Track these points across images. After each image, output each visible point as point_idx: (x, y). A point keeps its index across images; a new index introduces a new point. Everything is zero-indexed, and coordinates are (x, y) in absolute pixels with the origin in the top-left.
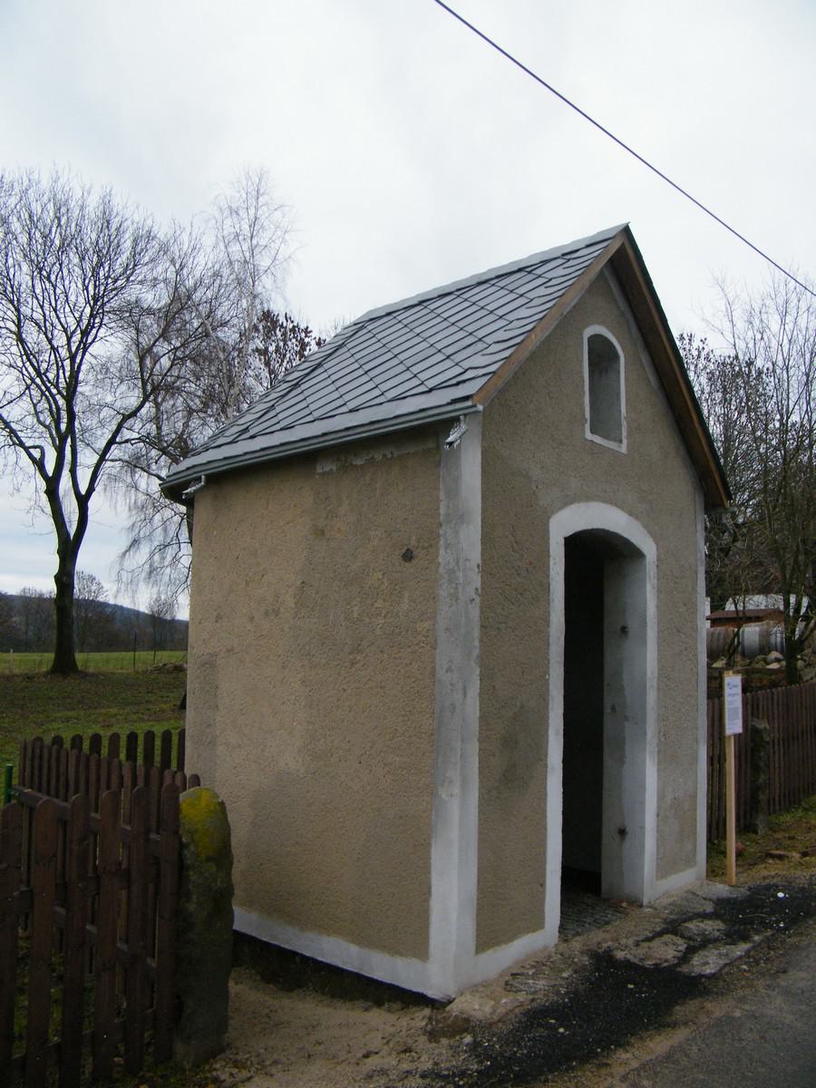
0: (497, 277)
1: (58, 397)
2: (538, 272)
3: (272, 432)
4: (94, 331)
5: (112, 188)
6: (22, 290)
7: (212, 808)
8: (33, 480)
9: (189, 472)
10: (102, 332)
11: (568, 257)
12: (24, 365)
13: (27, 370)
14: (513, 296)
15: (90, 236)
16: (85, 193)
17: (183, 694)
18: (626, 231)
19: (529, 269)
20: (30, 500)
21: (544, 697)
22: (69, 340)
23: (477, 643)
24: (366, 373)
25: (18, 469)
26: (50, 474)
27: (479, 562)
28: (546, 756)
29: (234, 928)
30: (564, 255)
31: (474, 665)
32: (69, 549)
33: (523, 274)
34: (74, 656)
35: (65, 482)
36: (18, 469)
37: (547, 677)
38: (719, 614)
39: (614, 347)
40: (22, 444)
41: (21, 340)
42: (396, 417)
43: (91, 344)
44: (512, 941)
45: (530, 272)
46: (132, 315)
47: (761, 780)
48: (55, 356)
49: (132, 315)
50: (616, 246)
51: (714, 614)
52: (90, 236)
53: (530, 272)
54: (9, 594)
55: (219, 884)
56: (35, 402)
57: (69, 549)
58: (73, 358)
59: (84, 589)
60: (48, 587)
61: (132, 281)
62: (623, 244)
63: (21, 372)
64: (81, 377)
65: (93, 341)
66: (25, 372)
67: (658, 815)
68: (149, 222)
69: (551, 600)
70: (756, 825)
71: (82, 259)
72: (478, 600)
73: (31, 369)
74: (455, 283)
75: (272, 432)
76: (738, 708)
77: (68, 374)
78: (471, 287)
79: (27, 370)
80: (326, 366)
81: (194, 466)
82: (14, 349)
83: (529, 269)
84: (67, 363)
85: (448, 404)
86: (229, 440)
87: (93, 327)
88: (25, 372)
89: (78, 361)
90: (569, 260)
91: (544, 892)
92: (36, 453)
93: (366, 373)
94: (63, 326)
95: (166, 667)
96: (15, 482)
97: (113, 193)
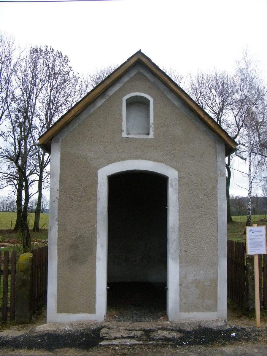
7: (27, 258)
17: (244, 230)
18: (140, 52)
21: (94, 233)
23: (56, 214)
27: (58, 188)
28: (96, 254)
31: (55, 221)
34: (231, 217)
37: (96, 226)
39: (136, 96)
44: (77, 313)
54: (244, 197)
55: (24, 278)
67: (181, 285)
69: (98, 199)
72: (57, 201)
76: (262, 242)
91: (95, 301)
95: (265, 219)
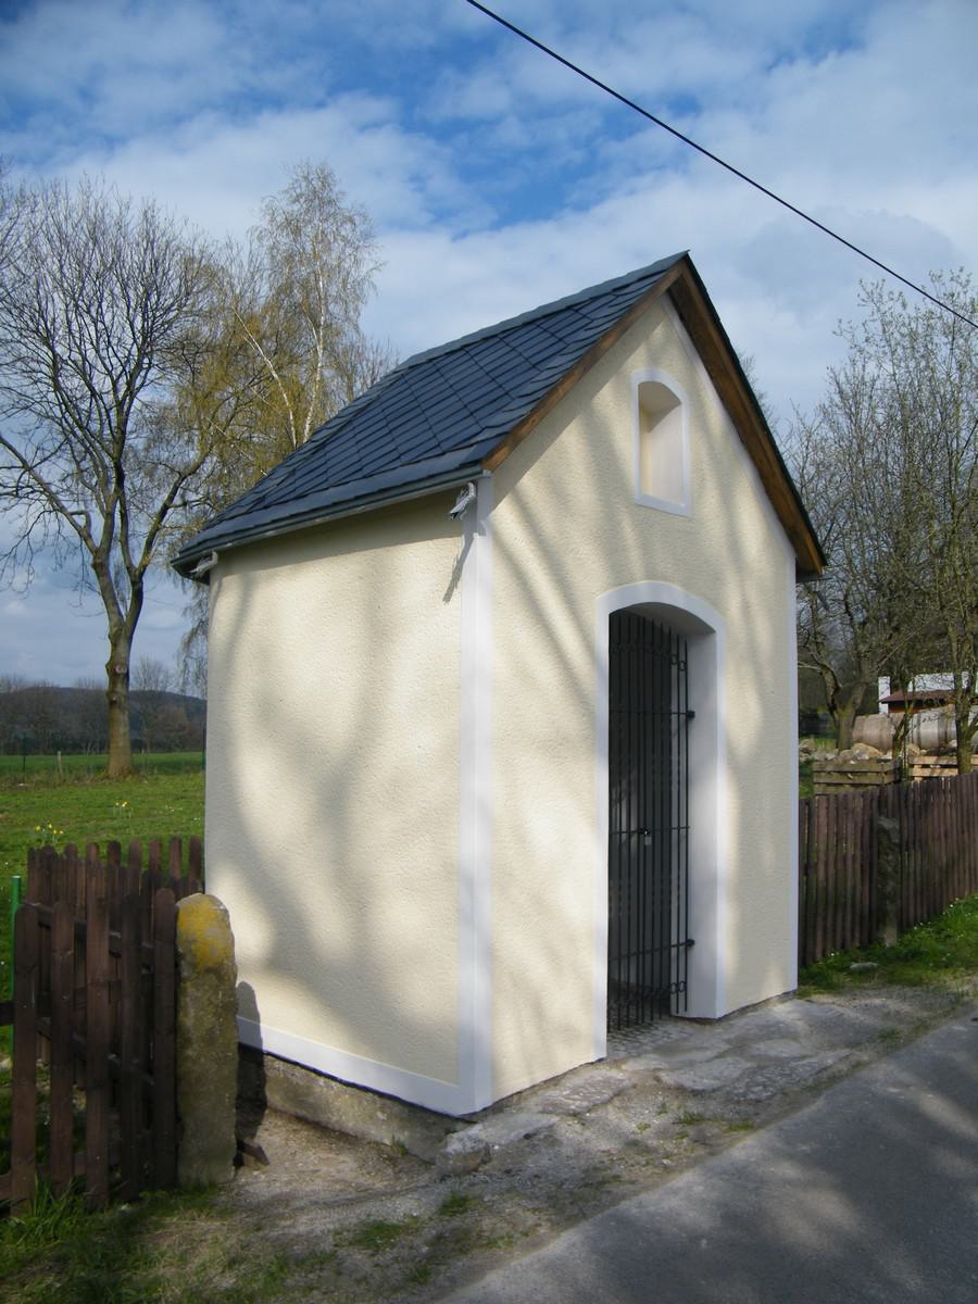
0: (544, 317)
1: (104, 454)
2: (584, 311)
3: (286, 502)
4: (143, 374)
5: (155, 201)
6: (57, 326)
8: (78, 552)
9: (200, 548)
10: (153, 373)
11: (618, 293)
12: (64, 417)
13: (67, 422)
14: (553, 340)
15: (132, 258)
16: (123, 208)
18: (685, 260)
19: (576, 308)
20: (76, 575)
22: (115, 383)
24: (472, 414)
25: (61, 538)
26: (98, 544)
29: (12, 1026)
30: (615, 290)
32: (122, 634)
33: (571, 312)
35: (116, 555)
36: (61, 538)
38: (898, 695)
40: (62, 509)
41: (57, 388)
42: (405, 484)
43: (138, 389)
45: (577, 311)
46: (187, 353)
47: (889, 889)
48: (98, 406)
49: (187, 353)
50: (673, 276)
51: (895, 694)
52: (132, 258)
53: (577, 311)
56: (78, 459)
57: (122, 634)
58: (120, 404)
59: (150, 679)
60: (99, 676)
61: (186, 312)
62: (682, 276)
63: (61, 425)
64: (130, 426)
65: (142, 385)
66: (65, 424)
68: (200, 241)
70: (883, 939)
71: (125, 287)
73: (70, 420)
74: (482, 330)
75: (286, 502)
77: (114, 424)
78: (539, 319)
79: (67, 422)
80: (355, 424)
81: (205, 541)
82: (51, 396)
83: (576, 308)
84: (113, 413)
85: (457, 469)
86: (244, 510)
87: (142, 369)
88: (65, 424)
89: (125, 408)
90: (618, 296)
92: (81, 521)
93: (472, 414)
94: (107, 370)
96: (58, 555)
97: (158, 205)
